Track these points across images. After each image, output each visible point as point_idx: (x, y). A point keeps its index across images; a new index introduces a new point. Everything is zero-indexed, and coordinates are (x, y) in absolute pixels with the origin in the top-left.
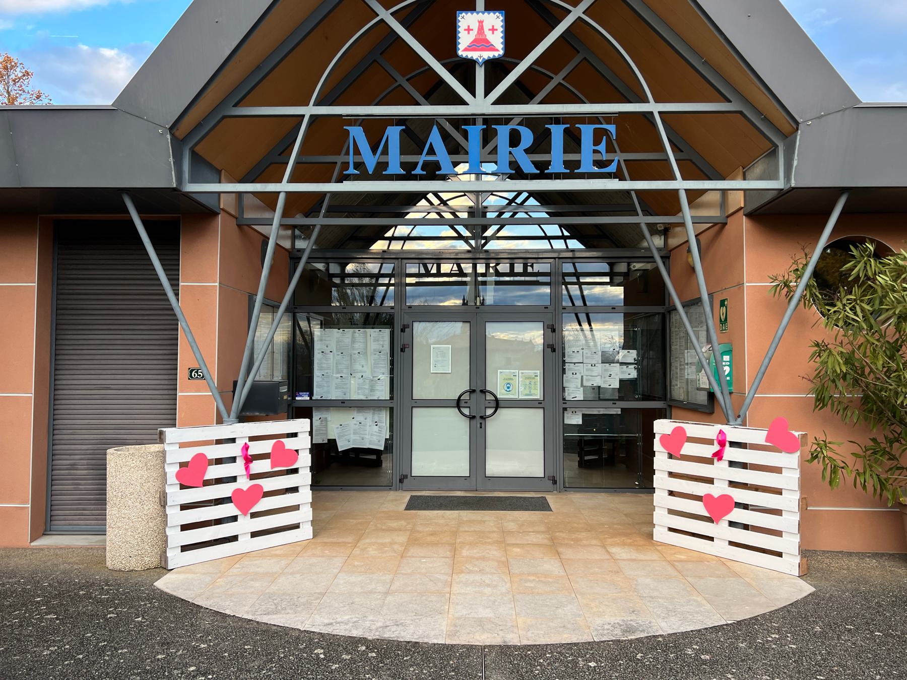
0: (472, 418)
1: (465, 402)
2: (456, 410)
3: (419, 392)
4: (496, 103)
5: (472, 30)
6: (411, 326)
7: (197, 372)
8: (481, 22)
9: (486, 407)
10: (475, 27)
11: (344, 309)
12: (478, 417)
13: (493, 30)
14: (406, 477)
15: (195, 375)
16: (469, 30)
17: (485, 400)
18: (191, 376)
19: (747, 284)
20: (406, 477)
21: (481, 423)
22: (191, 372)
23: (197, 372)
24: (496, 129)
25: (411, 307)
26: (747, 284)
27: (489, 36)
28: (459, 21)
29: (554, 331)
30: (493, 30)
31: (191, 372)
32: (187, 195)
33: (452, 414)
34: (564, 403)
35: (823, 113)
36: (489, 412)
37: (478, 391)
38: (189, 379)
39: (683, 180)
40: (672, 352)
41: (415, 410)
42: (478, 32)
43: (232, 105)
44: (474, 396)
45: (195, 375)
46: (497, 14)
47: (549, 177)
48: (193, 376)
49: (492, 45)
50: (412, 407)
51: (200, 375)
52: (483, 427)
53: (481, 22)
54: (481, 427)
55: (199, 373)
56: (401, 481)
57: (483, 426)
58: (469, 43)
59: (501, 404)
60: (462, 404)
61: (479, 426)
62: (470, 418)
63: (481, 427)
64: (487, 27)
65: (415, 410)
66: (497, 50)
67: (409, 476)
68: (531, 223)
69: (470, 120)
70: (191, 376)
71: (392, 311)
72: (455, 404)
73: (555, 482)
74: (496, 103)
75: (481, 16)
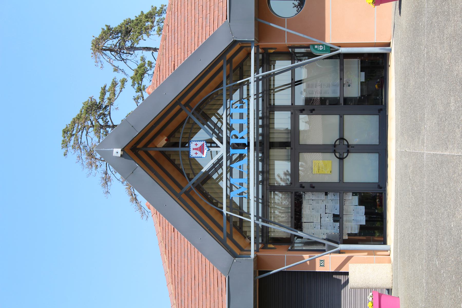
0: (348, 152)
1: (341, 155)
2: (344, 160)
3: (335, 178)
4: (222, 143)
5: (196, 152)
6: (301, 183)
7: (321, 263)
8: (194, 149)
9: (343, 145)
10: (195, 151)
11: (293, 217)
12: (348, 149)
13: (196, 145)
14: (379, 186)
15: (323, 264)
16: (196, 153)
17: (340, 145)
18: (323, 266)
19: (286, 42)
20: (379, 186)
21: (352, 147)
22: (321, 266)
23: (321, 263)
24: (232, 144)
25: (292, 183)
26: (286, 42)
27: (198, 146)
28: (193, 157)
29: (304, 110)
30: (196, 145)
31: (321, 266)
32: (254, 259)
33: (345, 160)
34: (341, 105)
35: (235, 261)
36: (338, 155)
37: (348, 149)
38: (324, 266)
39: (251, 77)
40: (312, 115)
41: (300, 144)
42: (197, 150)
43: (232, 72)
44: (337, 150)
45: (323, 264)
46: (190, 143)
47: (249, 143)
48: (323, 265)
49: (202, 145)
50: (299, 145)
51: (323, 262)
52: (353, 146)
53: (194, 149)
54: (354, 147)
55: (322, 262)
56: (381, 188)
57: (353, 146)
58: (201, 153)
59: (341, 137)
60: (341, 157)
61: (353, 148)
62: (349, 152)
63: (354, 147)
64: (195, 147)
65: (300, 144)
66: (204, 143)
67: (378, 184)
68: (340, 167)
69: (228, 151)
70: (323, 266)
71: (294, 193)
72: (341, 160)
73: (381, 110)
74: (222, 143)
75: (191, 149)
